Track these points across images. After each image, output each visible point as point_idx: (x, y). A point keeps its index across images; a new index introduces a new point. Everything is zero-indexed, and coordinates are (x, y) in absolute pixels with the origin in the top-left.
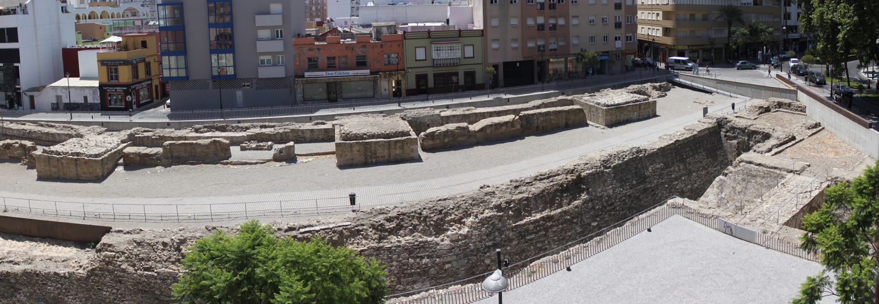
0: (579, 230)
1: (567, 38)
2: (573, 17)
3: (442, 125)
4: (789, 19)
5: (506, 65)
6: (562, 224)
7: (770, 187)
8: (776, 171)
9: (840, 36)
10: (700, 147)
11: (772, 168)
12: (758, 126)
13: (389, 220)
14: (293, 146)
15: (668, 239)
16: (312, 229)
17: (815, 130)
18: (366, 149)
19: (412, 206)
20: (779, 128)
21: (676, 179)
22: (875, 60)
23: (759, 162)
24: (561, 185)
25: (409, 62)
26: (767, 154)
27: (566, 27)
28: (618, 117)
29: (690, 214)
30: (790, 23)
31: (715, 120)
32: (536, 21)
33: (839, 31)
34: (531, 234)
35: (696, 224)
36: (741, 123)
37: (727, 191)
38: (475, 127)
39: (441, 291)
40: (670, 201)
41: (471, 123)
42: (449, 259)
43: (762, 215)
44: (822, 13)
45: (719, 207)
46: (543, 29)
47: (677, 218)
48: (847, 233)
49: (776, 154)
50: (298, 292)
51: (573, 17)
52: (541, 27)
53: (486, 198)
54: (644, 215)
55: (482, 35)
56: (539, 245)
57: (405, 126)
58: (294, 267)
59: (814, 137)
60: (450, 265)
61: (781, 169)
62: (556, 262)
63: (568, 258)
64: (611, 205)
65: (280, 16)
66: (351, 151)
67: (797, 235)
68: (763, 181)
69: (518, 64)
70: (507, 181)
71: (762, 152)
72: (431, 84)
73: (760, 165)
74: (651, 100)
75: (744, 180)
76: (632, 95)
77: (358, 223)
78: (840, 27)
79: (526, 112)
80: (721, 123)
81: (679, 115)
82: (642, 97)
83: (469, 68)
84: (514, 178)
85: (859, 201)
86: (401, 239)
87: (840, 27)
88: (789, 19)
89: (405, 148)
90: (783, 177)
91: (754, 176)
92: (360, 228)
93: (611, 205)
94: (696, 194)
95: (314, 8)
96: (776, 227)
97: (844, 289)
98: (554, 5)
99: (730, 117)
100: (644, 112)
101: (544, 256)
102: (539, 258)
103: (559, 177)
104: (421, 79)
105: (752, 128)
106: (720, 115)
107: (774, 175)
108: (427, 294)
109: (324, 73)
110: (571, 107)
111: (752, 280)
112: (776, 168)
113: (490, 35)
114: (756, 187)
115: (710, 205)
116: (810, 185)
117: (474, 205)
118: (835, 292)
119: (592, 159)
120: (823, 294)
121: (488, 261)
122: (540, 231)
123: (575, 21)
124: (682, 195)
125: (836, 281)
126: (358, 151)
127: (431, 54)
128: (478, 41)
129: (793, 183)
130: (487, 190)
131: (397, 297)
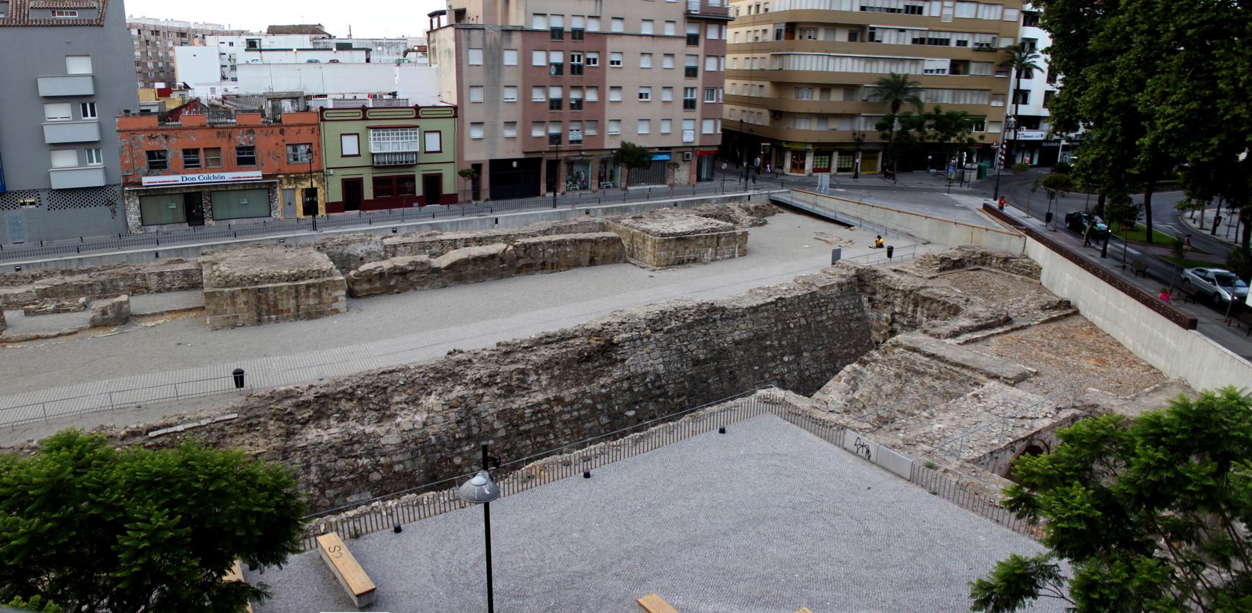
0: (604, 420)
1: (597, 122)
2: (613, 88)
4: (1025, 102)
6: (578, 410)
7: (947, 396)
11: (957, 365)
12: (936, 291)
13: (299, 406)
14: (128, 302)
15: (754, 452)
16: (170, 430)
17: (1055, 314)
18: (259, 299)
19: (338, 384)
20: (979, 299)
21: (774, 358)
23: (932, 351)
24: (580, 353)
25: (331, 159)
26: (948, 341)
27: (600, 104)
28: (681, 251)
29: (794, 416)
30: (1023, 110)
31: (853, 272)
32: (547, 94)
34: (528, 423)
35: (805, 433)
37: (864, 390)
38: (443, 262)
39: (390, 503)
40: (761, 392)
42: (400, 457)
45: (847, 412)
46: (559, 107)
47: (771, 420)
49: (967, 342)
50: (160, 528)
51: (613, 88)
52: (556, 104)
54: (715, 408)
55: (456, 116)
57: (322, 262)
58: (148, 490)
60: (401, 466)
61: (974, 370)
62: (567, 464)
64: (659, 388)
65: (90, 79)
66: (234, 304)
67: (998, 487)
68: (937, 384)
69: (515, 164)
70: (491, 344)
71: (939, 336)
72: (368, 194)
73: (933, 356)
74: (739, 231)
75: (898, 376)
76: (706, 220)
77: (249, 414)
78: (1146, 124)
79: (526, 241)
81: (786, 258)
82: (723, 223)
83: (431, 169)
84: (502, 340)
85: (1147, 454)
86: (323, 433)
87: (1146, 124)
88: (1025, 102)
89: (324, 295)
90: (977, 384)
91: (918, 373)
92: (255, 421)
93: (659, 388)
94: (808, 386)
95: (150, 65)
96: (954, 464)
97: (1086, 588)
99: (883, 270)
100: (725, 244)
101: (547, 455)
102: (541, 458)
103: (577, 342)
104: (352, 188)
106: (863, 263)
107: (958, 379)
108: (369, 509)
109: (178, 179)
110: (600, 234)
112: (964, 366)
113: (469, 115)
114: (921, 391)
115: (832, 407)
116: (1039, 410)
119: (633, 316)
121: (458, 461)
122: (543, 418)
123: (614, 96)
124: (783, 385)
126: (246, 303)
128: (447, 126)
131: (321, 516)
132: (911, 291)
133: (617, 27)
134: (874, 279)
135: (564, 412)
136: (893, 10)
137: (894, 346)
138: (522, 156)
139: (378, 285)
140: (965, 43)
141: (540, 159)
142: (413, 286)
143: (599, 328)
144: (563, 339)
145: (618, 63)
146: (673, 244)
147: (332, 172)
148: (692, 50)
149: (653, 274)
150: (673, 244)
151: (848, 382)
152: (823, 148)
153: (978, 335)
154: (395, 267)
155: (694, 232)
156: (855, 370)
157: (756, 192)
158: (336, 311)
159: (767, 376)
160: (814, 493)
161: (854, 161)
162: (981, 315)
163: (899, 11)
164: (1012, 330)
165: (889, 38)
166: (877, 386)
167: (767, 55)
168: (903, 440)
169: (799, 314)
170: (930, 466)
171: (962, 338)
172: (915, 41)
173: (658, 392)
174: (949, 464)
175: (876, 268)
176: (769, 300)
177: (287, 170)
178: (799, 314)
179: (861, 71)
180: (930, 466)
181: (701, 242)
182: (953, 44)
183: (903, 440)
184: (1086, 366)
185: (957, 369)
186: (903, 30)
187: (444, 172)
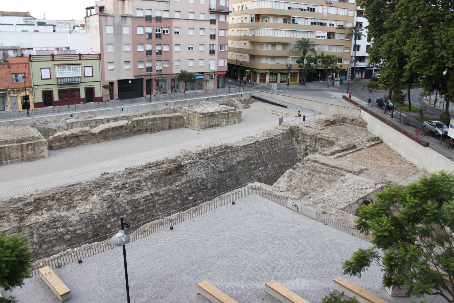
1: (168, 61)
3: (67, 130)
4: (358, 50)
5: (120, 82)
6: (166, 198)
7: (330, 181)
8: (337, 170)
9: (407, 67)
11: (334, 167)
12: (324, 135)
15: (248, 212)
17: (373, 143)
19: (46, 193)
20: (342, 138)
21: (255, 169)
22: (439, 90)
23: (323, 162)
24: (166, 171)
25: (36, 81)
26: (330, 157)
27: (170, 52)
28: (211, 121)
29: (265, 194)
30: (358, 54)
31: (288, 128)
32: (145, 48)
33: (406, 63)
34: (142, 206)
35: (270, 202)
36: (311, 132)
37: (295, 181)
38: (97, 130)
39: (75, 249)
41: (92, 127)
43: (323, 201)
44: (391, 46)
45: (288, 191)
46: (150, 54)
47: (255, 197)
48: (397, 223)
49: (338, 157)
51: (176, 44)
52: (149, 53)
53: (106, 182)
54: (230, 193)
55: (100, 59)
56: (148, 213)
57: (35, 132)
59: (373, 148)
60: (80, 231)
61: (341, 169)
62: (162, 224)
63: (171, 221)
67: (353, 220)
68: (326, 176)
69: (130, 82)
71: (326, 155)
72: (56, 98)
73: (324, 164)
74: (237, 111)
75: (309, 174)
76: (222, 106)
79: (138, 119)
80: (292, 132)
82: (230, 108)
83: (89, 85)
86: (39, 217)
88: (358, 50)
89: (36, 149)
90: (342, 175)
91: (318, 172)
93: (203, 185)
96: (334, 211)
98: (160, 35)
99: (301, 126)
101: (152, 220)
103: (164, 166)
105: (318, 136)
106: (293, 124)
107: (335, 173)
108: (65, 253)
111: (312, 245)
112: (337, 168)
113: (106, 58)
115: (281, 189)
116: (367, 185)
117: (97, 188)
118: (381, 263)
119: (190, 152)
120: (371, 263)
122: (149, 203)
123: (177, 48)
124: (260, 180)
125: (383, 256)
127: (55, 73)
128: (95, 64)
129: (352, 181)
130: (107, 176)
131: (40, 258)
132: (314, 136)
133: (177, 15)
134: (298, 131)
135: (160, 200)
136: (302, 10)
137: (307, 160)
138: (134, 78)
139: (64, 143)
140: (333, 25)
141: (142, 79)
142: (82, 143)
143: (174, 159)
144: (157, 165)
146: (207, 118)
147: (36, 87)
148: (213, 26)
149: (198, 132)
150: (207, 118)
151: (288, 178)
152: (274, 72)
153: (342, 154)
154: (73, 134)
155: (217, 112)
156: (291, 172)
157: (244, 93)
158: (43, 157)
159: (252, 177)
160: (275, 228)
161: (287, 78)
162: (343, 145)
163: (305, 10)
164: (356, 151)
165: (301, 22)
166: (300, 178)
167: (247, 29)
168: (312, 202)
169: (265, 148)
170: (324, 213)
171: (336, 155)
172: (312, 23)
173: (203, 187)
174: (332, 211)
175: (298, 125)
176: (252, 142)
177: (12, 86)
178: (265, 148)
179: (289, 36)
180: (324, 213)
181: (220, 116)
182: (328, 25)
183: (312, 202)
184: (386, 165)
185: (334, 169)
187: (95, 86)
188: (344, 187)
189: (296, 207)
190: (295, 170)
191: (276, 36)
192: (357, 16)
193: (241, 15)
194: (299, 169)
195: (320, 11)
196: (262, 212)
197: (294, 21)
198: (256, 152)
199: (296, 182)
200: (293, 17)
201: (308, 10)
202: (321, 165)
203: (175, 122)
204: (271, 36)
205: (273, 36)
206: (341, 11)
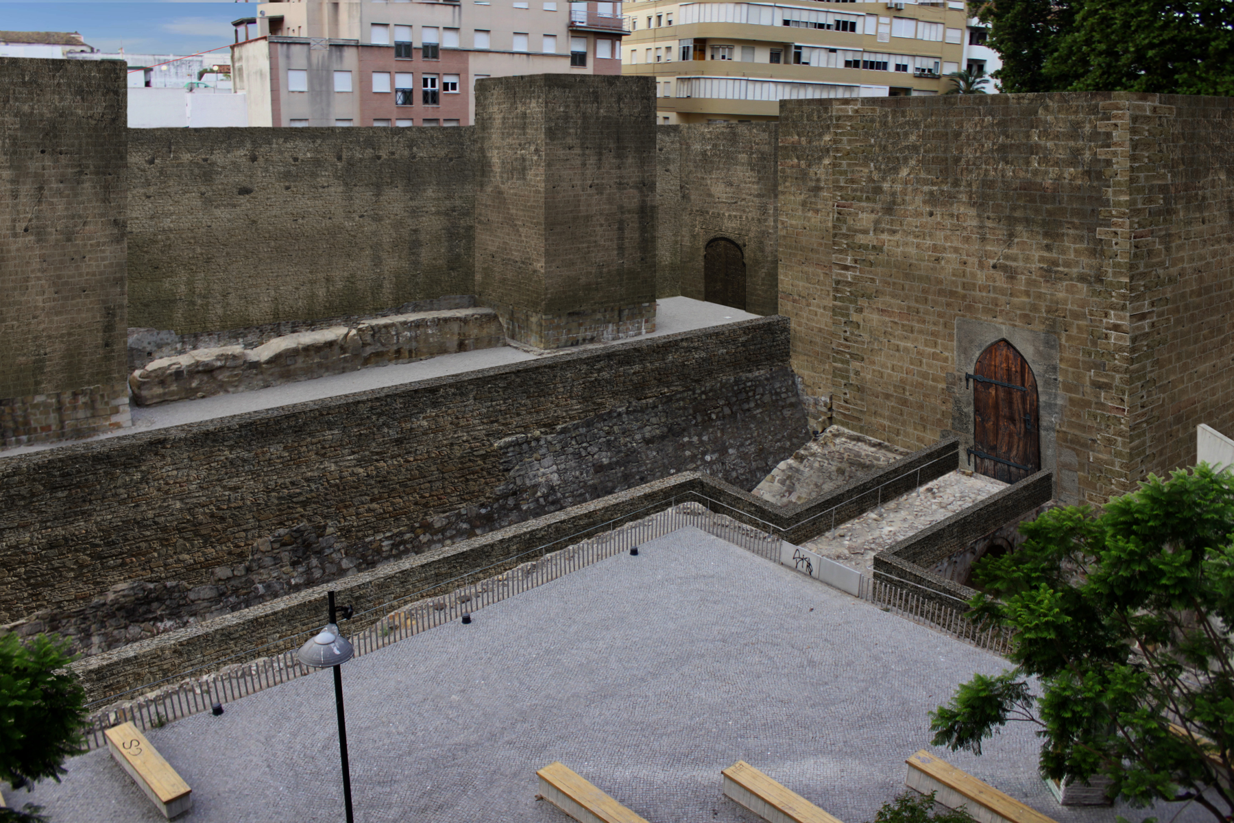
10: (747, 400)
35: (734, 548)
62: (440, 608)
98: (435, 94)
120: (1008, 715)
125: (1041, 695)
133: (481, 42)
136: (821, 26)
140: (905, 68)
145: (454, 86)
151: (783, 482)
156: (791, 468)
160: (748, 620)
163: (829, 27)
166: (816, 485)
169: (722, 402)
172: (848, 63)
178: (722, 402)
182: (891, 68)
183: (849, 548)
186: (834, 51)
188: (934, 507)
189: (805, 564)
190: (801, 462)
191: (750, 98)
192: (971, 43)
193: (655, 39)
194: (811, 459)
195: (870, 30)
196: (713, 577)
197: (798, 58)
198: (695, 412)
199: (804, 496)
200: (797, 47)
201: (837, 29)
202: (873, 449)
203: (476, 331)
204: (736, 97)
205: (743, 97)
206: (927, 32)
